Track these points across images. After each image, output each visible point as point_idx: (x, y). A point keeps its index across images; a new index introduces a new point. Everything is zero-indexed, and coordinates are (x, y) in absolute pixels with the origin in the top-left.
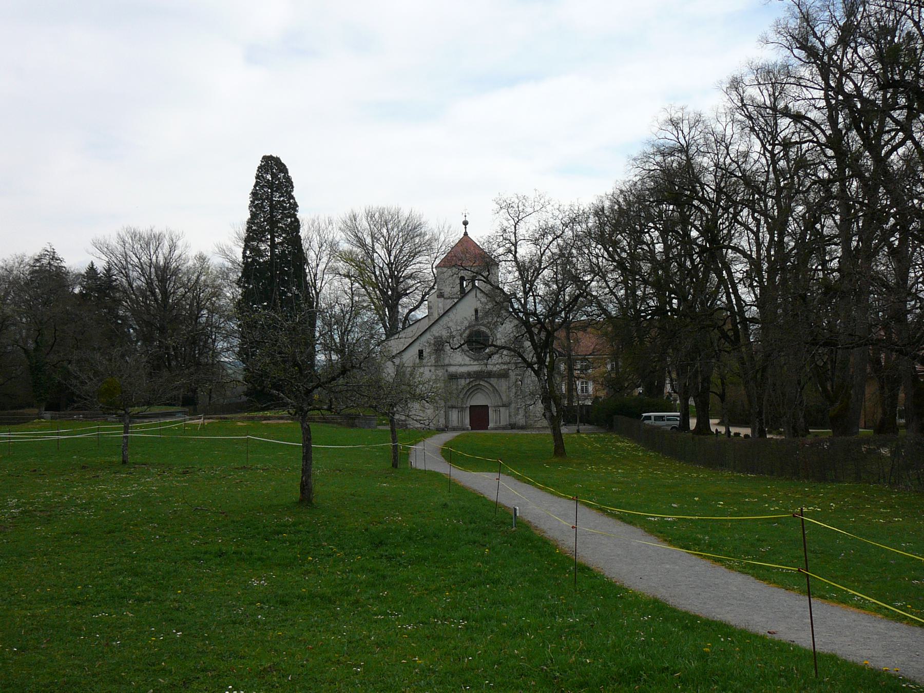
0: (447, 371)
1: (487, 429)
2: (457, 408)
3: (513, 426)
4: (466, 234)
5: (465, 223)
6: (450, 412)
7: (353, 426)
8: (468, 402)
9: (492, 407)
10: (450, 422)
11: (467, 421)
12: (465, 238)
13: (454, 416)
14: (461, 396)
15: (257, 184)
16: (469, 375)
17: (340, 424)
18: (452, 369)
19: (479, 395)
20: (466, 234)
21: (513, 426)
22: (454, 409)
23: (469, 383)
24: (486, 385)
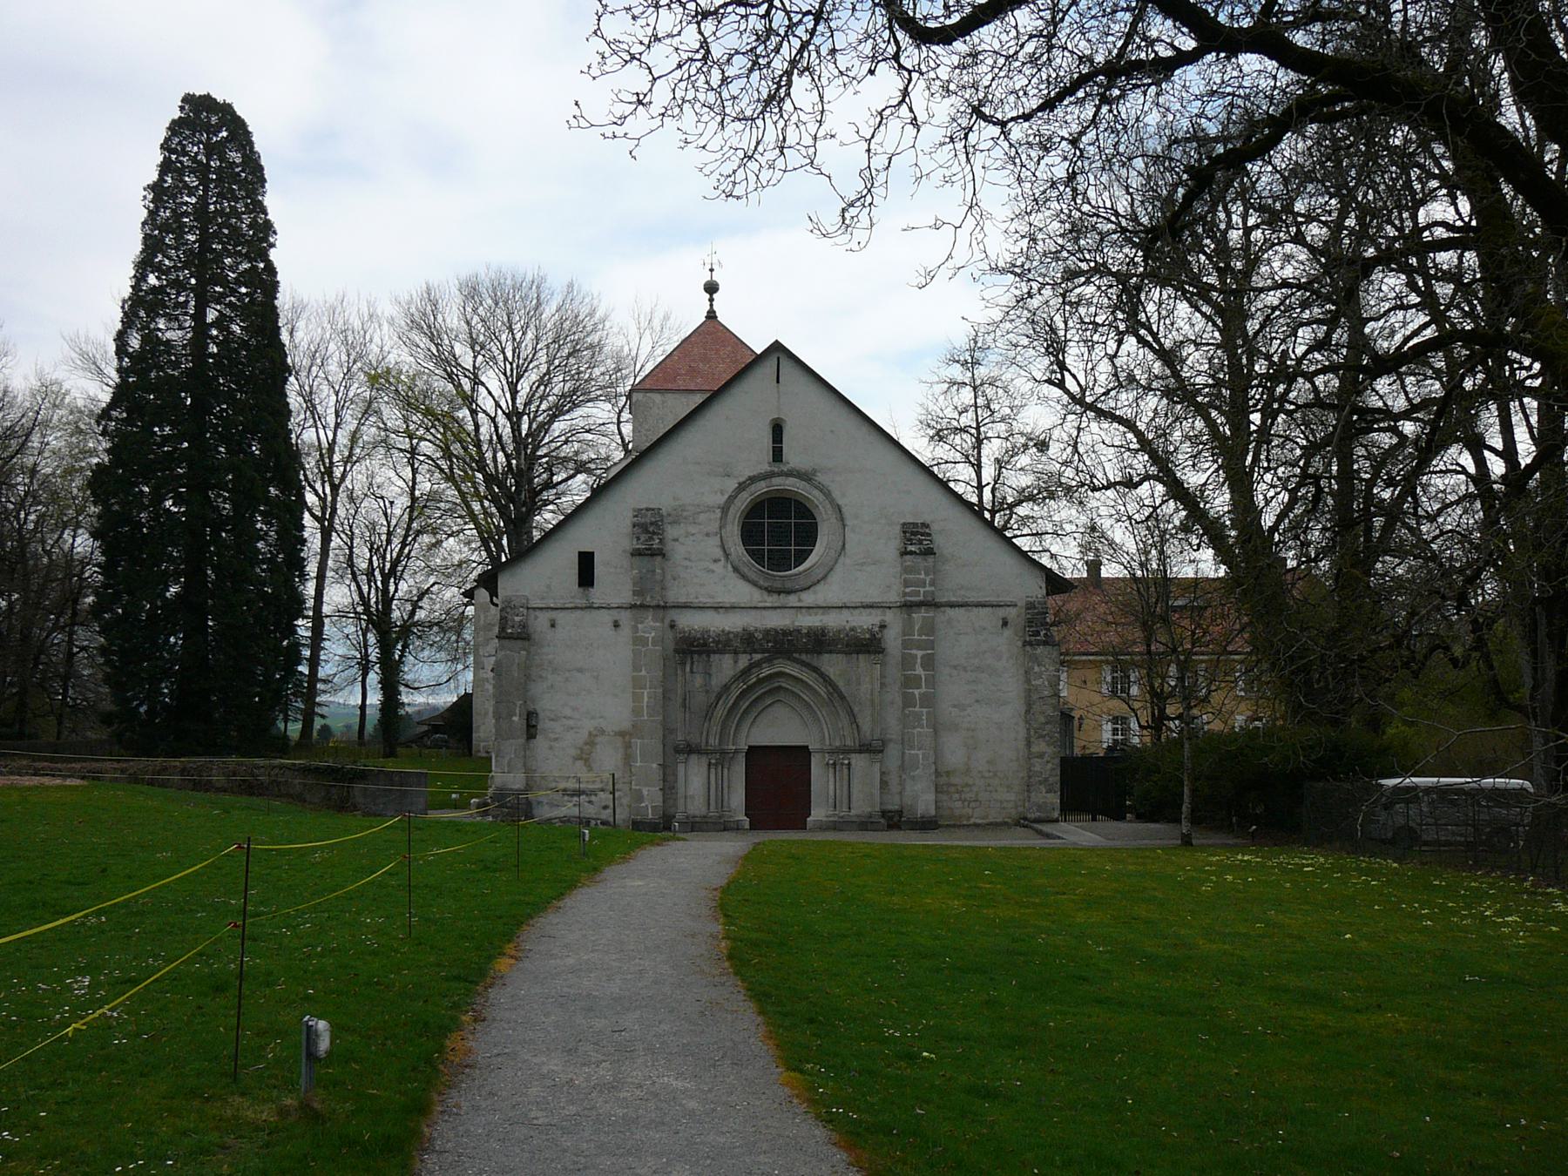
0: (672, 626)
1: (803, 827)
2: (706, 753)
3: (894, 820)
4: (711, 315)
5: (711, 288)
6: (681, 768)
7: (343, 806)
8: (744, 734)
9: (822, 751)
10: (681, 802)
11: (737, 799)
12: (711, 323)
13: (695, 780)
14: (720, 712)
15: (165, 167)
16: (747, 640)
17: (301, 799)
18: (692, 622)
19: (780, 712)
20: (711, 315)
21: (894, 820)
22: (694, 758)
23: (746, 672)
24: (805, 676)
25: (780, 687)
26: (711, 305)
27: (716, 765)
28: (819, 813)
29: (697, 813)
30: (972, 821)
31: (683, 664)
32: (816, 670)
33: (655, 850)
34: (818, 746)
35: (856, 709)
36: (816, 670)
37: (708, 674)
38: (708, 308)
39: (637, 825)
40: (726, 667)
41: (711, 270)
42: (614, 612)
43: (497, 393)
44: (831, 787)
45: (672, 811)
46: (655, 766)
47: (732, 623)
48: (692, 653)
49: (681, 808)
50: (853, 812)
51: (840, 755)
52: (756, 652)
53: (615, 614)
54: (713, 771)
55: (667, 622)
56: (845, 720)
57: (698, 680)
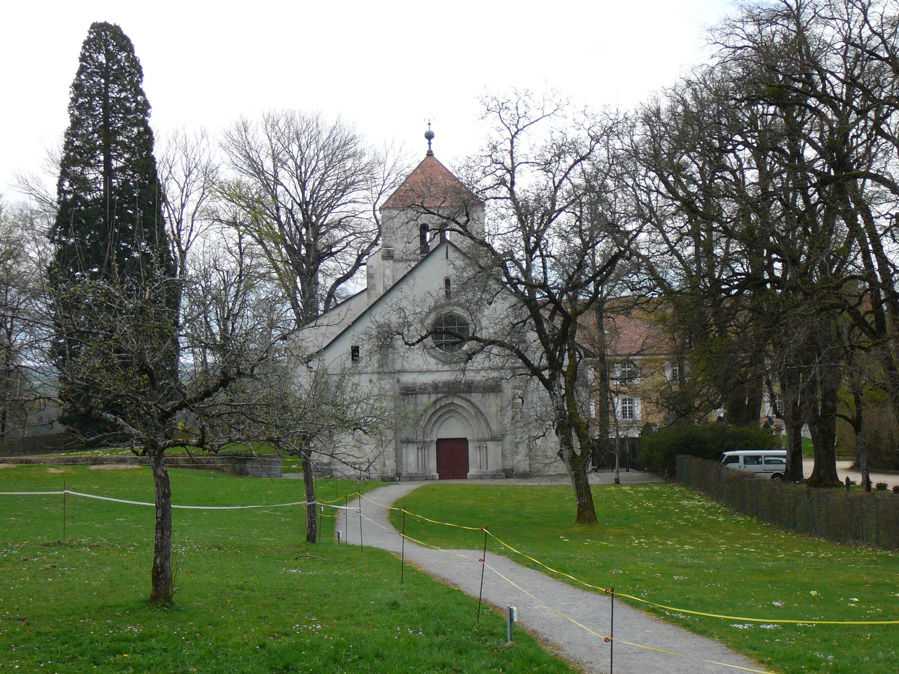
1: (466, 478)
3: (508, 473)
4: (430, 154)
5: (429, 136)
6: (404, 450)
7: (242, 473)
9: (473, 441)
11: (433, 464)
13: (411, 456)
15: (82, 70)
16: (435, 387)
17: (220, 470)
19: (452, 422)
20: (430, 154)
21: (508, 473)
22: (410, 445)
23: (435, 403)
25: (452, 410)
26: (430, 147)
27: (421, 448)
28: (472, 471)
29: (413, 472)
30: (549, 473)
31: (404, 400)
32: (468, 401)
33: (384, 488)
34: (472, 438)
35: (489, 420)
36: (468, 401)
37: (416, 404)
38: (428, 149)
39: (383, 479)
40: (425, 400)
41: (429, 124)
42: (370, 375)
43: (291, 188)
44: (478, 458)
45: (401, 471)
46: (391, 450)
47: (427, 379)
48: (408, 394)
49: (405, 470)
50: (489, 470)
51: (482, 442)
52: (439, 393)
53: (370, 376)
54: (420, 451)
55: (395, 380)
56: (483, 424)
57: (411, 407)
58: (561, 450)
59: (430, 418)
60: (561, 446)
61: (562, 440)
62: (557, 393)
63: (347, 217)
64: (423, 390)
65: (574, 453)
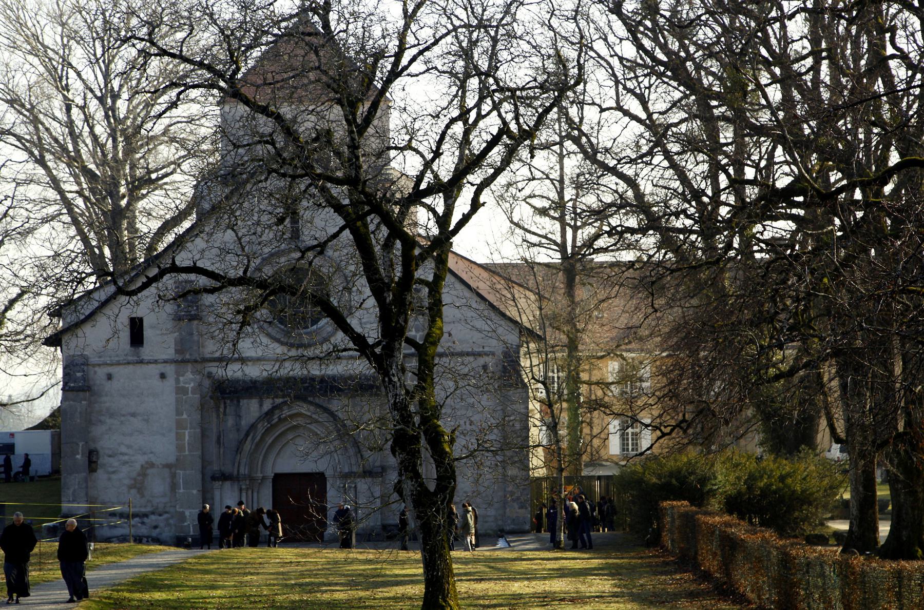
22: (228, 484)
23: (270, 413)
32: (326, 410)
36: (326, 410)
40: (252, 409)
46: (195, 492)
52: (277, 397)
53: (160, 368)
58: (399, 482)
59: (262, 439)
60: (400, 475)
61: (402, 462)
62: (396, 379)
63: (178, 122)
64: (252, 388)
65: (422, 485)
